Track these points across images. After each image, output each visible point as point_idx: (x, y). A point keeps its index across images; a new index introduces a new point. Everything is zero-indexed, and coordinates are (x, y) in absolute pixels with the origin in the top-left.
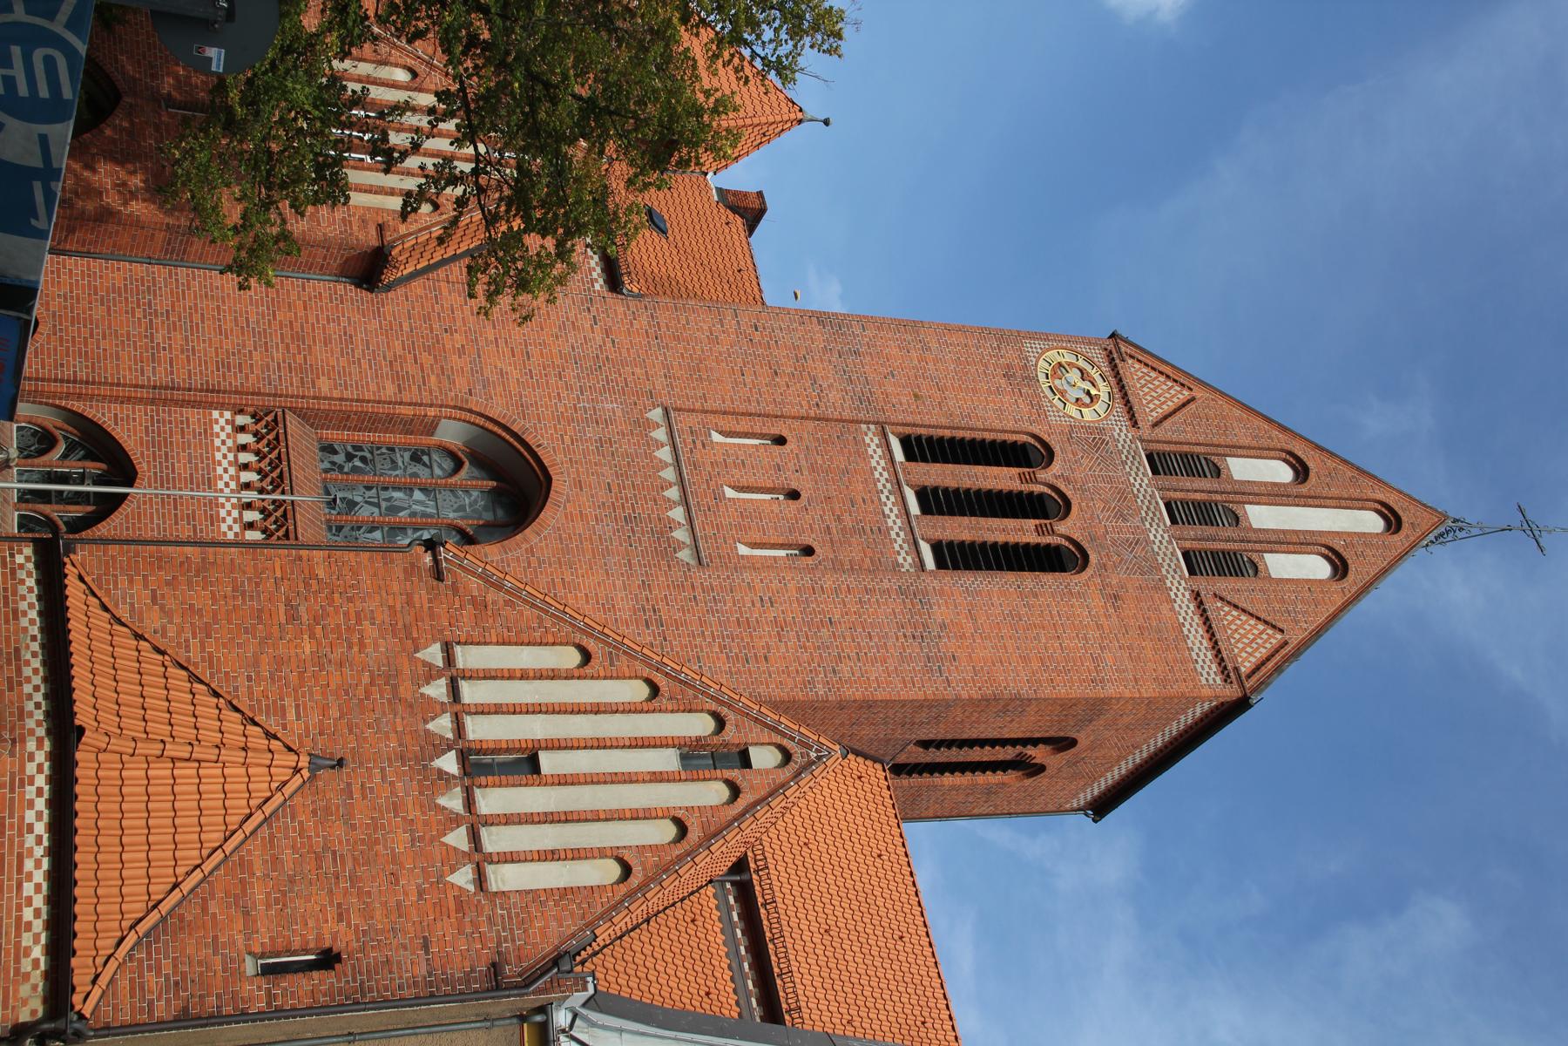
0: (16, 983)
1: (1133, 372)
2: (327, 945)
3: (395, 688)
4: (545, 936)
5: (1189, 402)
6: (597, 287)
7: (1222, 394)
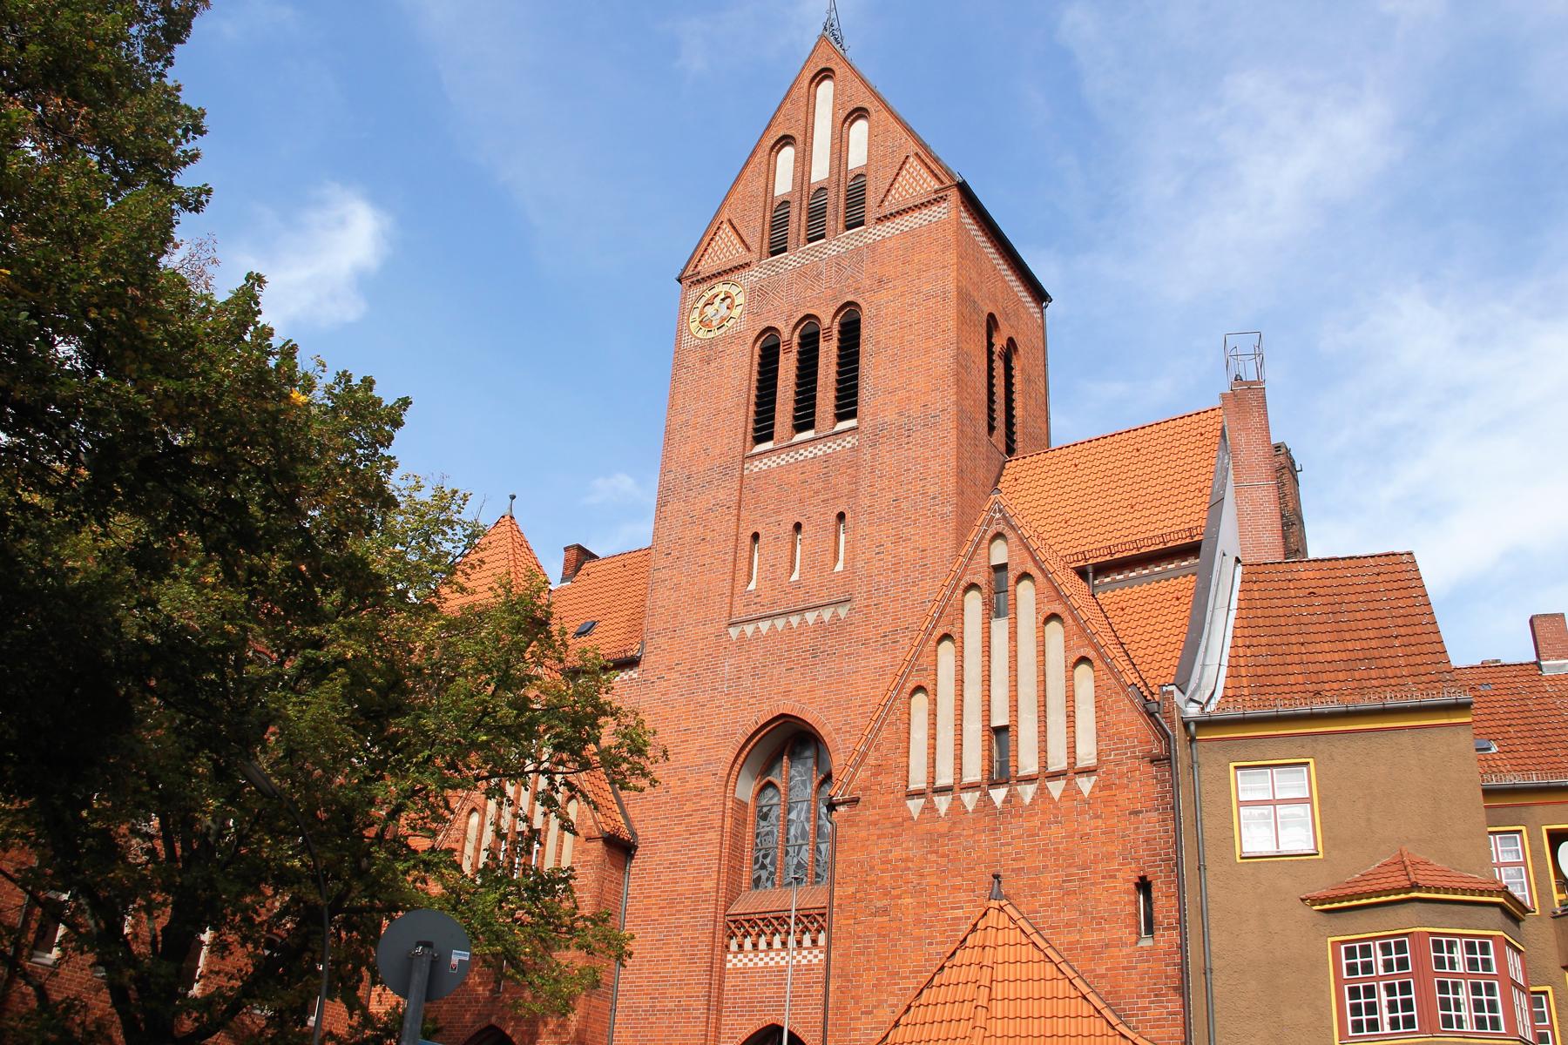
1: (707, 266)
3: (940, 835)
4: (1132, 724)
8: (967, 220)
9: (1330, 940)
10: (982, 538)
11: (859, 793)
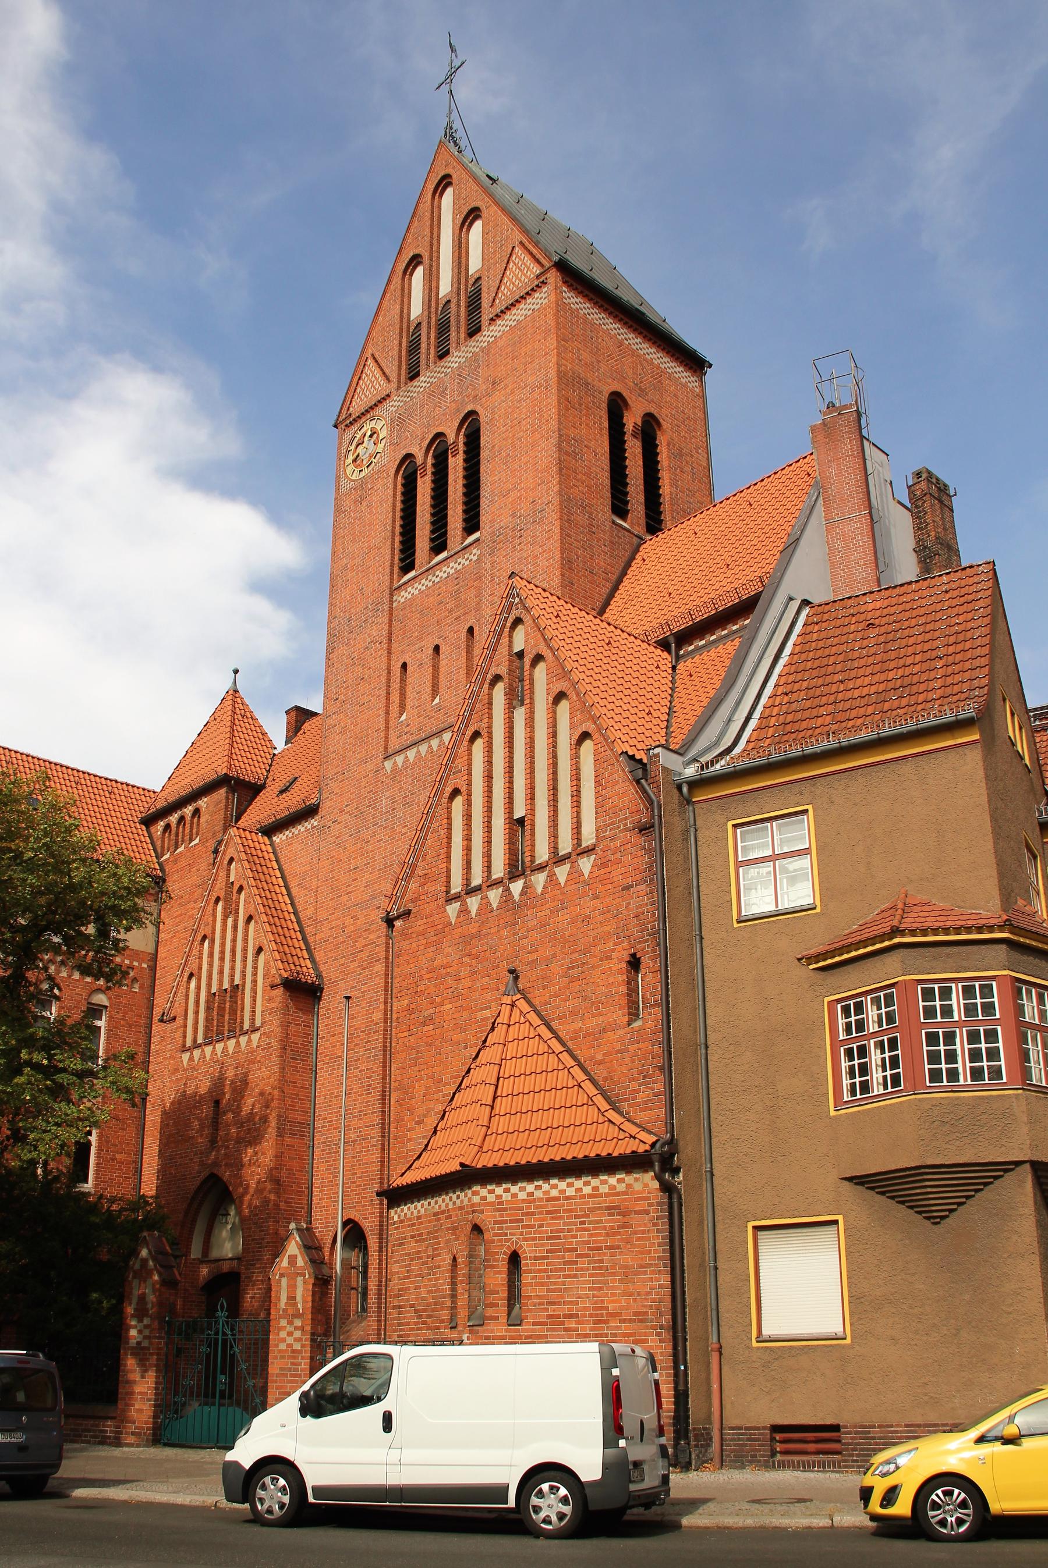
0: (632, 1193)
1: (358, 405)
2: (624, 965)
3: (473, 937)
4: (624, 791)
5: (374, 358)
6: (316, 824)
7: (369, 334)
8: (574, 301)
9: (826, 1000)
10: (504, 626)
11: (410, 906)
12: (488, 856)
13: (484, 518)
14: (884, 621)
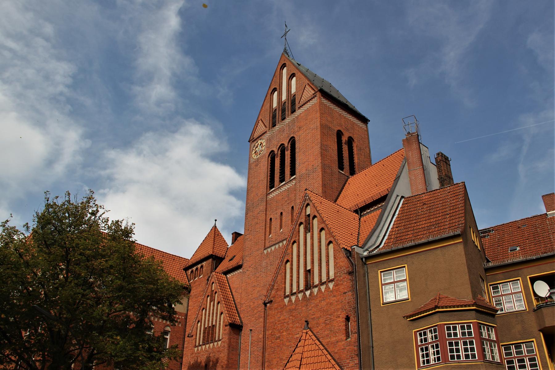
1: (256, 135)
3: (293, 310)
4: (344, 262)
8: (325, 101)
9: (414, 331)
12: (298, 282)
13: (297, 171)
14: (429, 202)
